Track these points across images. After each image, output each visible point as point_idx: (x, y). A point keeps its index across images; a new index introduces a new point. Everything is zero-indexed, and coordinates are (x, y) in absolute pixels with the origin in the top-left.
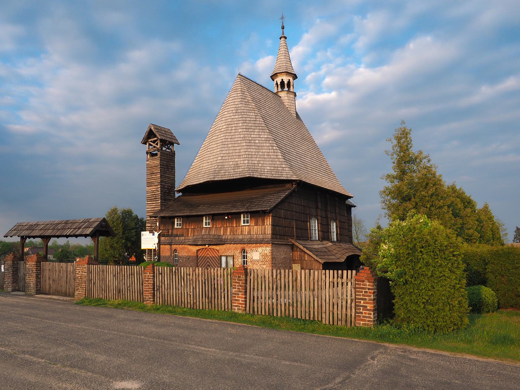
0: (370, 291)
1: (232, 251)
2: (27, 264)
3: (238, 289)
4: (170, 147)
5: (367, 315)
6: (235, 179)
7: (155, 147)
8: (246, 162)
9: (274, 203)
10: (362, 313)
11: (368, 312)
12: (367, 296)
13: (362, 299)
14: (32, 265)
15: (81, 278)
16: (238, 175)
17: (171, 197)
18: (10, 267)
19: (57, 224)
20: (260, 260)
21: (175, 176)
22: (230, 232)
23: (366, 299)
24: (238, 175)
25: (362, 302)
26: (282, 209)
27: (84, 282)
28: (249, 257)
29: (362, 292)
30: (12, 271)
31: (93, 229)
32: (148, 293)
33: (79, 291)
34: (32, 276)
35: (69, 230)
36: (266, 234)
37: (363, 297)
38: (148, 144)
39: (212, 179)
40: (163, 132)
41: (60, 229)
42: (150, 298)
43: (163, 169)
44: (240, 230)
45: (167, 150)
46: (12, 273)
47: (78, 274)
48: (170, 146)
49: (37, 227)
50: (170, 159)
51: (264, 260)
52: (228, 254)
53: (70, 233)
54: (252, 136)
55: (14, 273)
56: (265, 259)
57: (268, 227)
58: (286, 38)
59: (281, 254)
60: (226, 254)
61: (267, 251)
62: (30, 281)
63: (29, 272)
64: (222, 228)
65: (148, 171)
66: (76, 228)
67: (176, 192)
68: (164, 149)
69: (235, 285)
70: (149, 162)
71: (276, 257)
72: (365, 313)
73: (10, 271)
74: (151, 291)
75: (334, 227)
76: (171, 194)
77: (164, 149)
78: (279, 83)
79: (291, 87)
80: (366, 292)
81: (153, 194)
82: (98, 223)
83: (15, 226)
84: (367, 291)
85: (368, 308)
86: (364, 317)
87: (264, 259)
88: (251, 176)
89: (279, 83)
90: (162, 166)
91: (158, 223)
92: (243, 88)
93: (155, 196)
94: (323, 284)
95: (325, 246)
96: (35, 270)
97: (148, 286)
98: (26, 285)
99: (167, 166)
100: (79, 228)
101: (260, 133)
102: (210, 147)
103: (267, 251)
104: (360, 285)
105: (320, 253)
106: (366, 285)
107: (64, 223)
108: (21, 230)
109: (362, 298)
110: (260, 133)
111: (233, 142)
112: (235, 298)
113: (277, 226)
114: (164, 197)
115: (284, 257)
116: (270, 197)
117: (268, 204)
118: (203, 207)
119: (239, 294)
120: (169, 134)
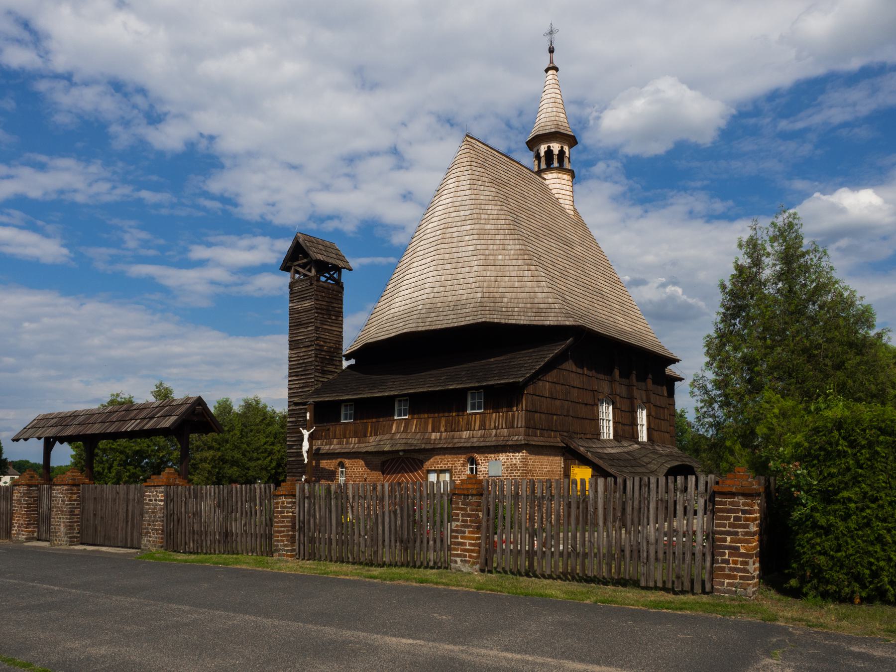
0: (748, 516)
1: (449, 461)
2: (54, 490)
3: (463, 521)
4: (335, 276)
5: (739, 566)
6: (457, 327)
7: (305, 275)
8: (479, 295)
9: (531, 369)
10: (727, 562)
11: (741, 559)
12: (740, 526)
13: (728, 533)
14: (63, 490)
15: (153, 513)
16: (463, 319)
17: (334, 367)
18: (22, 497)
19: (111, 412)
20: (503, 476)
21: (342, 328)
22: (446, 426)
23: (738, 532)
24: (463, 319)
25: (729, 539)
26: (546, 381)
27: (159, 519)
28: (481, 471)
29: (729, 518)
30: (28, 504)
31: (177, 417)
32: (281, 536)
33: (150, 537)
34: (63, 511)
35: (133, 421)
36: (515, 426)
37: (731, 530)
38: (293, 270)
39: (414, 330)
40: (321, 247)
41: (115, 422)
42: (286, 546)
43: (321, 316)
44: (465, 421)
45: (329, 281)
46: (27, 508)
47: (148, 504)
48: (334, 274)
49: (73, 419)
50: (334, 296)
51: (511, 476)
52: (441, 467)
53: (134, 427)
54: (491, 247)
55: (31, 507)
56: (513, 473)
57: (518, 413)
58: (557, 69)
59: (543, 465)
60: (438, 467)
61: (517, 460)
62: (58, 522)
63: (58, 504)
64: (430, 421)
65: (293, 321)
66: (145, 418)
67: (344, 358)
68: (323, 279)
69: (457, 515)
70: (294, 304)
71: (534, 471)
72: (735, 562)
73: (23, 504)
74: (288, 531)
75: (642, 417)
76: (335, 363)
77: (323, 279)
78: (542, 154)
79: (566, 160)
80: (737, 519)
81: (302, 361)
82: (188, 406)
83: (35, 420)
84: (741, 517)
85: (742, 551)
86: (731, 569)
87: (510, 473)
88: (488, 320)
89: (542, 154)
90: (319, 311)
91: (308, 414)
92: (474, 160)
93: (304, 365)
94: (642, 505)
95: (626, 450)
96: (68, 501)
97: (283, 522)
98: (52, 529)
99: (328, 310)
100: (151, 418)
101: (507, 242)
102: (409, 272)
103: (517, 460)
104: (724, 503)
105: (616, 461)
106: (737, 504)
107: (124, 411)
108: (43, 427)
109: (729, 531)
110: (507, 242)
111: (455, 260)
112: (456, 540)
113: (536, 412)
114: (322, 367)
115: (549, 471)
116: (524, 358)
117: (519, 372)
118: (394, 382)
119: (464, 532)
120: (333, 251)
